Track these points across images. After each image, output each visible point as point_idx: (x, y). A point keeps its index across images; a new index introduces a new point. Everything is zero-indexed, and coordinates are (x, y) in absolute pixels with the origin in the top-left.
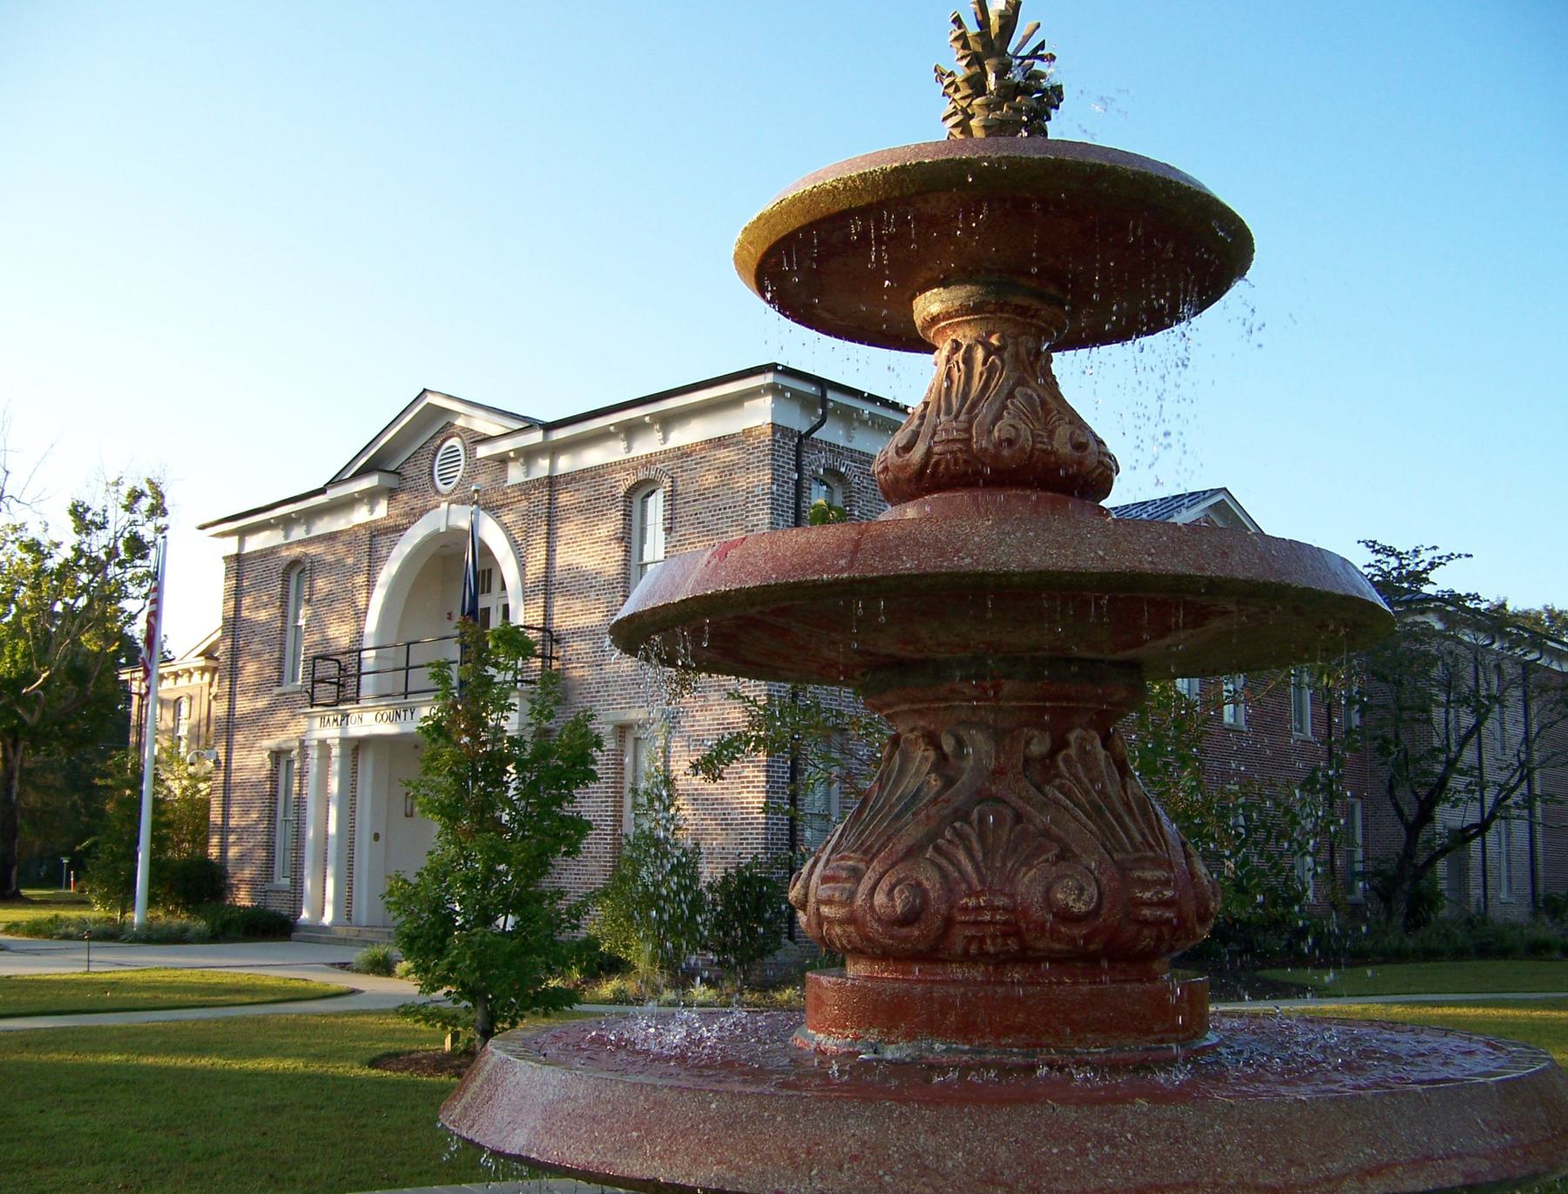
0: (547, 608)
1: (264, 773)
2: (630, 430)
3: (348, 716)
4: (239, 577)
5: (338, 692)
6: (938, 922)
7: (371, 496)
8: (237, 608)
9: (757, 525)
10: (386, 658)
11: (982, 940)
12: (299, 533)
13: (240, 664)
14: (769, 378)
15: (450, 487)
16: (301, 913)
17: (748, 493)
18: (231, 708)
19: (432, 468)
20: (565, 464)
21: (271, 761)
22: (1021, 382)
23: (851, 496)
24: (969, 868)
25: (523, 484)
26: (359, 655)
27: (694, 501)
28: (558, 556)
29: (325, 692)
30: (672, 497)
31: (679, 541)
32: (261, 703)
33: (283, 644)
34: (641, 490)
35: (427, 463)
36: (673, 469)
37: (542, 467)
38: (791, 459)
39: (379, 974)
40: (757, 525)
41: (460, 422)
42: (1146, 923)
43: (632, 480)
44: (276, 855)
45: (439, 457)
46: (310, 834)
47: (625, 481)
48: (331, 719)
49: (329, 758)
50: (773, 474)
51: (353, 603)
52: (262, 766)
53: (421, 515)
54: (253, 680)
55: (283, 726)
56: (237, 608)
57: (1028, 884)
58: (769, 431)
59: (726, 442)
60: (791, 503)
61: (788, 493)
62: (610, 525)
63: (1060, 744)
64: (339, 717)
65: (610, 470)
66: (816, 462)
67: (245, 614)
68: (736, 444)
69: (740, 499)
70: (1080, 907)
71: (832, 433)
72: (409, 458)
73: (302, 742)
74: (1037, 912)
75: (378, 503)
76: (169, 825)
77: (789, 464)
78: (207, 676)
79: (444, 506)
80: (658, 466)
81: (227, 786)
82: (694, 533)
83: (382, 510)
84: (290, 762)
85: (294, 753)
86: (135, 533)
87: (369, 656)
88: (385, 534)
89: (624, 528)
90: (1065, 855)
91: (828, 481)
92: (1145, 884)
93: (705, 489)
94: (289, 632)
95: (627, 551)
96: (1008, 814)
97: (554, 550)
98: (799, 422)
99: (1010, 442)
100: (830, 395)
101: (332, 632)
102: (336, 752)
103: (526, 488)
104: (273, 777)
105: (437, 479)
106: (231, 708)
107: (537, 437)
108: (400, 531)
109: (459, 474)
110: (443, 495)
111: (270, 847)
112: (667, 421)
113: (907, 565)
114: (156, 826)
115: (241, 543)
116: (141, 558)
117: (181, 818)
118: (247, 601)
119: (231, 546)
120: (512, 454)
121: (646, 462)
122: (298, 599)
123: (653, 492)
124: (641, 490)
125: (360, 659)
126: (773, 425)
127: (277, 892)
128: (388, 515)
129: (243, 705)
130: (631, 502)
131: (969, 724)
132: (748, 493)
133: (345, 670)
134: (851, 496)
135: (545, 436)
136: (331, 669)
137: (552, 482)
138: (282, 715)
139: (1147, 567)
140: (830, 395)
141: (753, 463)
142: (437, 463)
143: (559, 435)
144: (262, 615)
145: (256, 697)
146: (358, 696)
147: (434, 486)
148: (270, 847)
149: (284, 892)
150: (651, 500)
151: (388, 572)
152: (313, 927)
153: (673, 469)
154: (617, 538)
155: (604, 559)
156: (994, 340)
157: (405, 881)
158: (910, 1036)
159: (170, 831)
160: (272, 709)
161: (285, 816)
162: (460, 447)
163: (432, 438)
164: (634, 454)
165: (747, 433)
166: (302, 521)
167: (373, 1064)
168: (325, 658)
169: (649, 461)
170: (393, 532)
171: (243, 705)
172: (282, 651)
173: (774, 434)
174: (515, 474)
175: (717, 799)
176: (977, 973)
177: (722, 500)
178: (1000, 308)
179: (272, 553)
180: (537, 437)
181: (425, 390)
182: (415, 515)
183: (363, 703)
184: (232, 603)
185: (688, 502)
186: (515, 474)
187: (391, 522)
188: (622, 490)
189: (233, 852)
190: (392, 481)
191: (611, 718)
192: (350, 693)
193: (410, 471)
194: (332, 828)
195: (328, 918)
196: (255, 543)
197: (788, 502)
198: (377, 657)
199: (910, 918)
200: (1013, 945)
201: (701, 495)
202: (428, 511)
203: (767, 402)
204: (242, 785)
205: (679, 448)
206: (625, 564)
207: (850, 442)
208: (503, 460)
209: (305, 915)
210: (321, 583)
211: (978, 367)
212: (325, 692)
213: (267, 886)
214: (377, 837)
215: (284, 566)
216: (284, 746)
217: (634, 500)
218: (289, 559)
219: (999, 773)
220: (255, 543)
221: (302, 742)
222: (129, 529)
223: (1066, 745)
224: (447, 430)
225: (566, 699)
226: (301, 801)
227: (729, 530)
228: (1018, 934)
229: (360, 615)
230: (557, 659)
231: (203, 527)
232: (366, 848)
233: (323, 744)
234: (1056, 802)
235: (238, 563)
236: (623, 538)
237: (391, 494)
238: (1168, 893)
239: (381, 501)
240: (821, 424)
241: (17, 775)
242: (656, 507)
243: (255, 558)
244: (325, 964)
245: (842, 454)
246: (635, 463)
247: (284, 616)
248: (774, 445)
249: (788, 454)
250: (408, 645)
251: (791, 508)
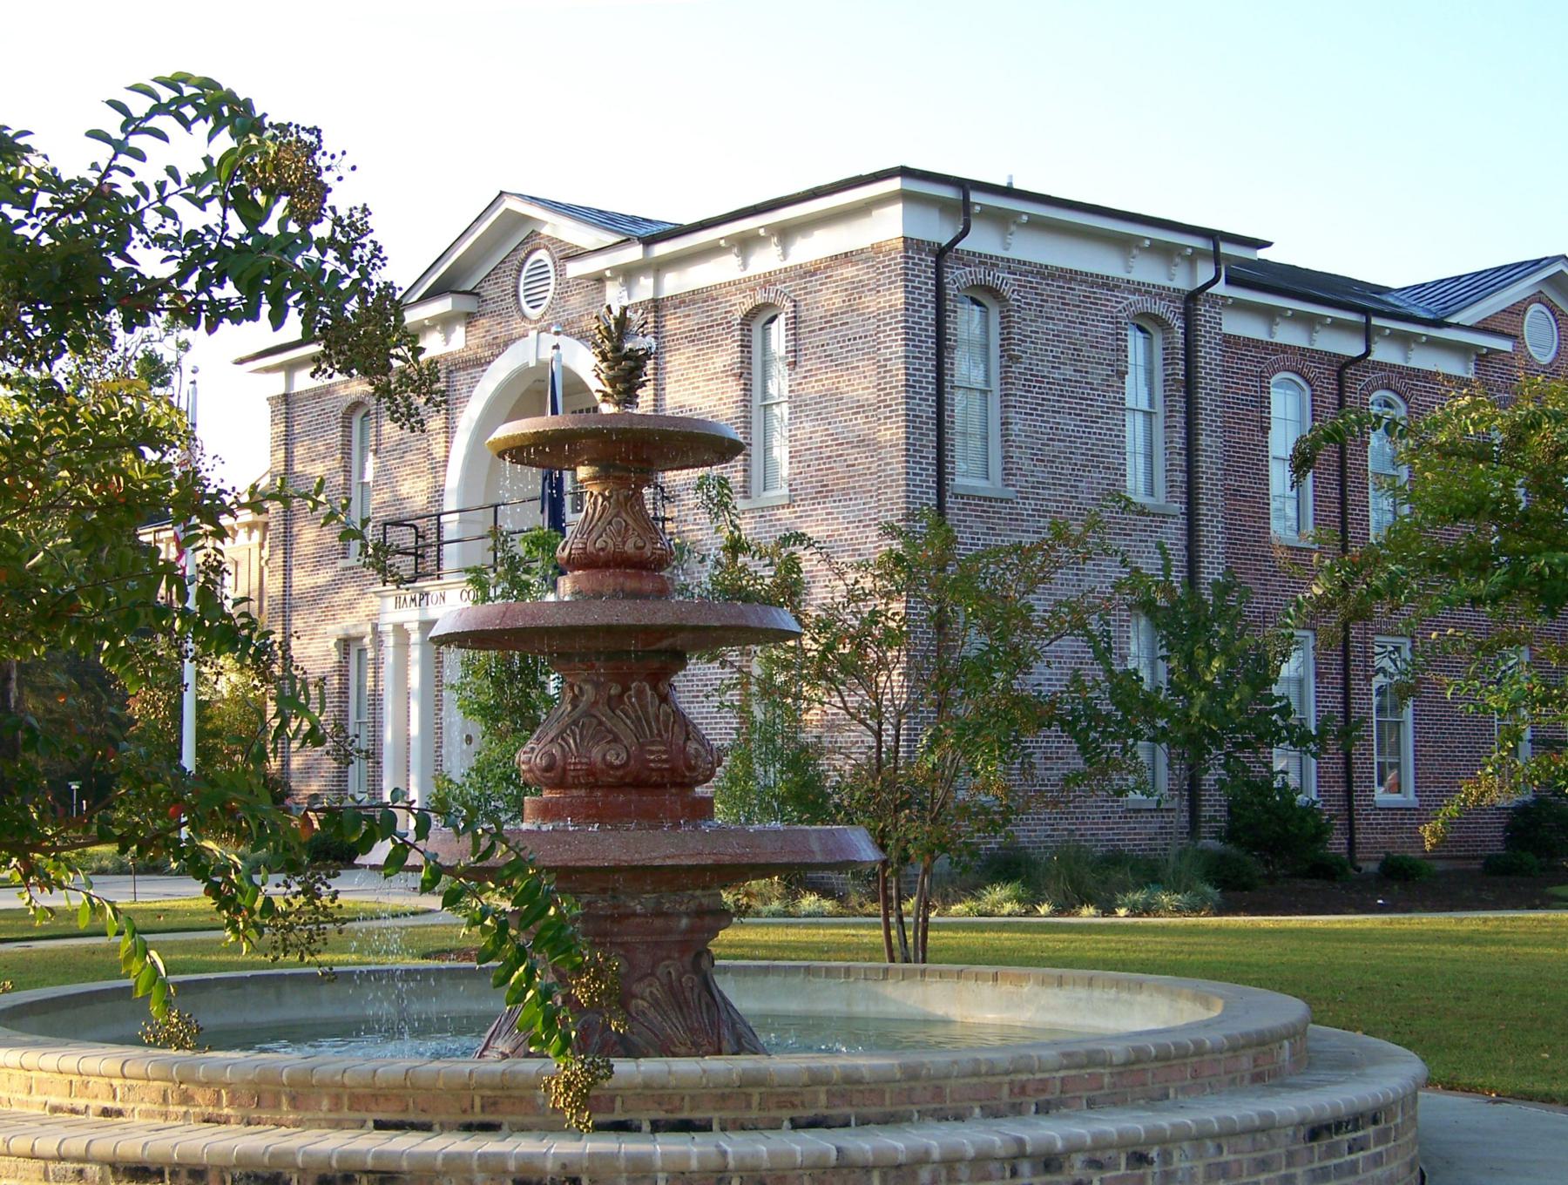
2: (745, 244)
3: (427, 594)
5: (416, 564)
6: (560, 770)
9: (890, 359)
10: (473, 522)
11: (578, 777)
13: (295, 530)
14: (895, 184)
15: (540, 311)
18: (287, 585)
19: (516, 287)
21: (339, 650)
22: (617, 515)
23: (1009, 316)
24: (573, 745)
26: (439, 519)
27: (821, 329)
28: (667, 397)
30: (795, 322)
31: (805, 377)
32: (324, 577)
34: (760, 315)
35: (510, 282)
36: (794, 291)
37: (645, 289)
38: (930, 278)
40: (890, 359)
42: (653, 770)
43: (748, 305)
46: (388, 735)
49: (408, 645)
50: (907, 298)
52: (328, 654)
53: (506, 345)
54: (310, 549)
55: (350, 605)
57: (596, 754)
58: (901, 245)
59: (854, 259)
60: (931, 331)
61: (927, 319)
62: (726, 355)
63: (626, 689)
65: (724, 291)
66: (957, 277)
67: (298, 468)
68: (866, 260)
69: (871, 326)
70: (617, 762)
71: (981, 240)
72: (489, 275)
73: (375, 627)
74: (600, 765)
75: (454, 331)
76: (216, 734)
77: (927, 284)
78: (256, 535)
79: (533, 334)
80: (779, 287)
82: (820, 368)
84: (362, 651)
85: (367, 641)
86: (153, 351)
87: (451, 525)
88: (464, 369)
89: (742, 362)
90: (616, 739)
91: (985, 302)
92: (652, 753)
93: (832, 315)
94: (353, 491)
95: (747, 389)
96: (595, 721)
98: (939, 231)
99: (602, 549)
100: (975, 197)
101: (405, 489)
102: (415, 637)
105: (523, 301)
106: (287, 585)
107: (634, 253)
108: (482, 365)
109: (549, 295)
110: (531, 321)
112: (785, 233)
113: (520, 624)
114: (201, 734)
115: (289, 381)
116: (160, 386)
117: (231, 725)
118: (299, 451)
119: (276, 384)
120: (608, 273)
121: (766, 282)
122: (363, 449)
123: (775, 317)
124: (760, 315)
125: (439, 523)
126: (905, 239)
128: (467, 346)
129: (302, 580)
130: (749, 330)
131: (586, 681)
133: (423, 537)
134: (1009, 316)
135: (645, 251)
136: (406, 538)
138: (349, 592)
139: (615, 622)
140: (975, 197)
141: (884, 284)
142: (522, 281)
143: (661, 249)
144: (318, 469)
145: (317, 567)
146: (439, 569)
147: (520, 309)
150: (774, 326)
153: (794, 291)
154: (734, 375)
156: (607, 493)
157: (450, 781)
158: (552, 820)
159: (218, 741)
160: (335, 585)
161: (358, 717)
162: (548, 261)
163: (514, 250)
164: (750, 272)
165: (877, 249)
167: (426, 956)
168: (398, 523)
169: (767, 281)
170: (474, 366)
171: (302, 580)
173: (906, 250)
176: (583, 792)
177: (851, 328)
178: (607, 478)
179: (328, 392)
180: (634, 253)
181: (502, 193)
182: (500, 346)
183: (447, 579)
184: (281, 455)
185: (813, 331)
187: (467, 354)
188: (738, 315)
189: (296, 762)
190: (468, 304)
192: (430, 565)
193: (490, 291)
194: (414, 729)
197: (927, 330)
198: (461, 521)
199: (549, 768)
200: (591, 779)
201: (828, 321)
202: (514, 340)
203: (896, 210)
205: (801, 266)
206: (746, 406)
207: (1007, 249)
208: (599, 279)
211: (599, 508)
215: (344, 409)
216: (353, 632)
217: (753, 327)
218: (349, 401)
219: (596, 703)
221: (375, 627)
222: (143, 346)
223: (630, 689)
224: (532, 240)
226: (376, 700)
227: (860, 364)
228: (593, 774)
230: (671, 519)
231: (241, 362)
233: (399, 629)
234: (619, 717)
235: (286, 403)
236: (741, 375)
237: (470, 319)
238: (664, 757)
239: (458, 327)
240: (964, 233)
241: (14, 675)
242: (778, 335)
245: (997, 266)
246: (752, 284)
247: (347, 470)
248: (907, 263)
249: (925, 272)
250: (496, 506)
251: (931, 337)
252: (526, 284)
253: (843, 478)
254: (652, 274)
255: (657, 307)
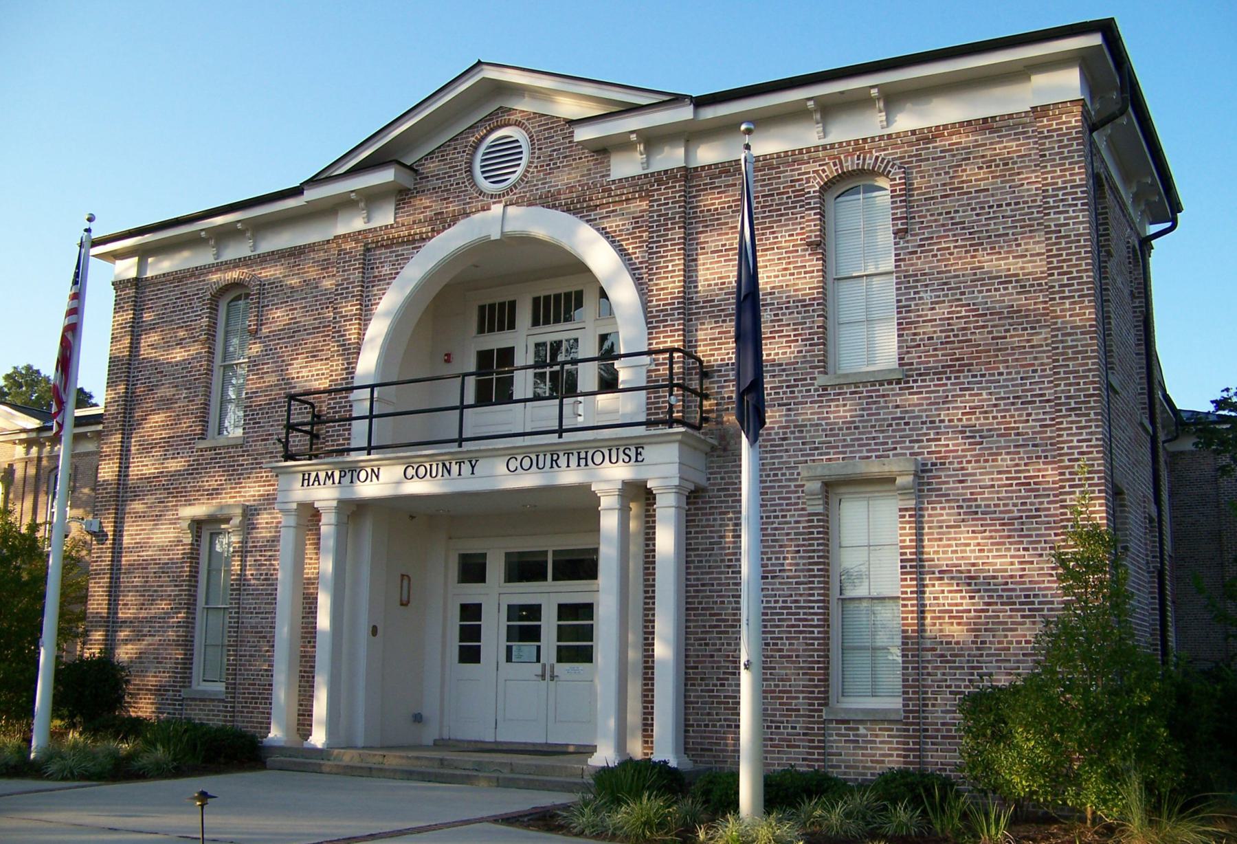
0: (688, 332)
1: (178, 553)
2: (828, 110)
4: (138, 309)
7: (371, 198)
8: (134, 346)
12: (233, 252)
13: (138, 414)
16: (268, 729)
17: (332, 371)
20: (707, 154)
25: (639, 177)
29: (298, 441)
33: (208, 387)
39: (539, 828)
41: (524, 106)
43: (831, 171)
44: (196, 653)
45: (482, 150)
47: (813, 177)
48: (322, 475)
51: (340, 333)
56: (134, 346)
64: (337, 474)
67: (145, 352)
81: (115, 569)
83: (385, 217)
94: (215, 374)
97: (696, 260)
103: (644, 185)
104: (193, 556)
111: (187, 643)
127: (202, 700)
132: (332, 371)
136: (300, 415)
137: (688, 174)
143: (710, 113)
147: (474, 184)
148: (187, 643)
149: (213, 700)
151: (390, 301)
152: (296, 749)
154: (809, 244)
155: (786, 269)
160: (194, 471)
161: (207, 603)
166: (248, 234)
172: (208, 394)
174: (625, 167)
175: (1011, 577)
181: (479, 63)
184: (127, 341)
186: (625, 167)
190: (407, 181)
191: (819, 472)
195: (318, 738)
196: (160, 266)
204: (132, 567)
209: (275, 734)
210: (279, 316)
212: (298, 441)
213: (184, 693)
214: (374, 631)
220: (160, 266)
225: (725, 450)
229: (351, 352)
232: (362, 651)
237: (401, 196)
243: (162, 283)
244: (496, 820)
252: (521, 159)
253: (247, 469)
254: (683, 143)
255: (686, 177)
